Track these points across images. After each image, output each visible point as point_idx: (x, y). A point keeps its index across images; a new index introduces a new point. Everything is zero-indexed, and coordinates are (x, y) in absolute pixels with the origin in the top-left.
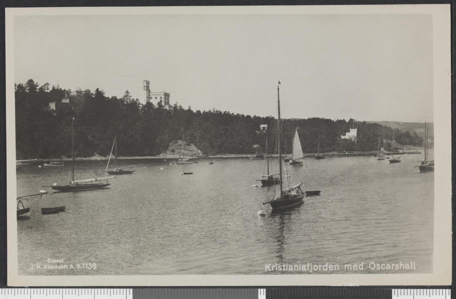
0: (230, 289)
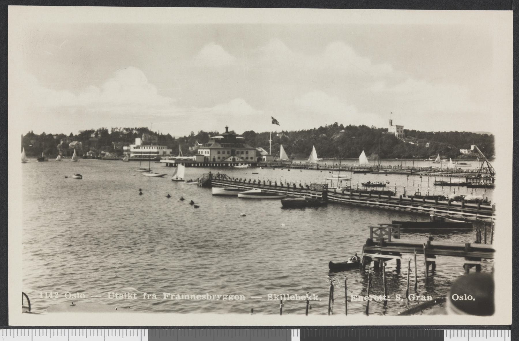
0: (259, 330)
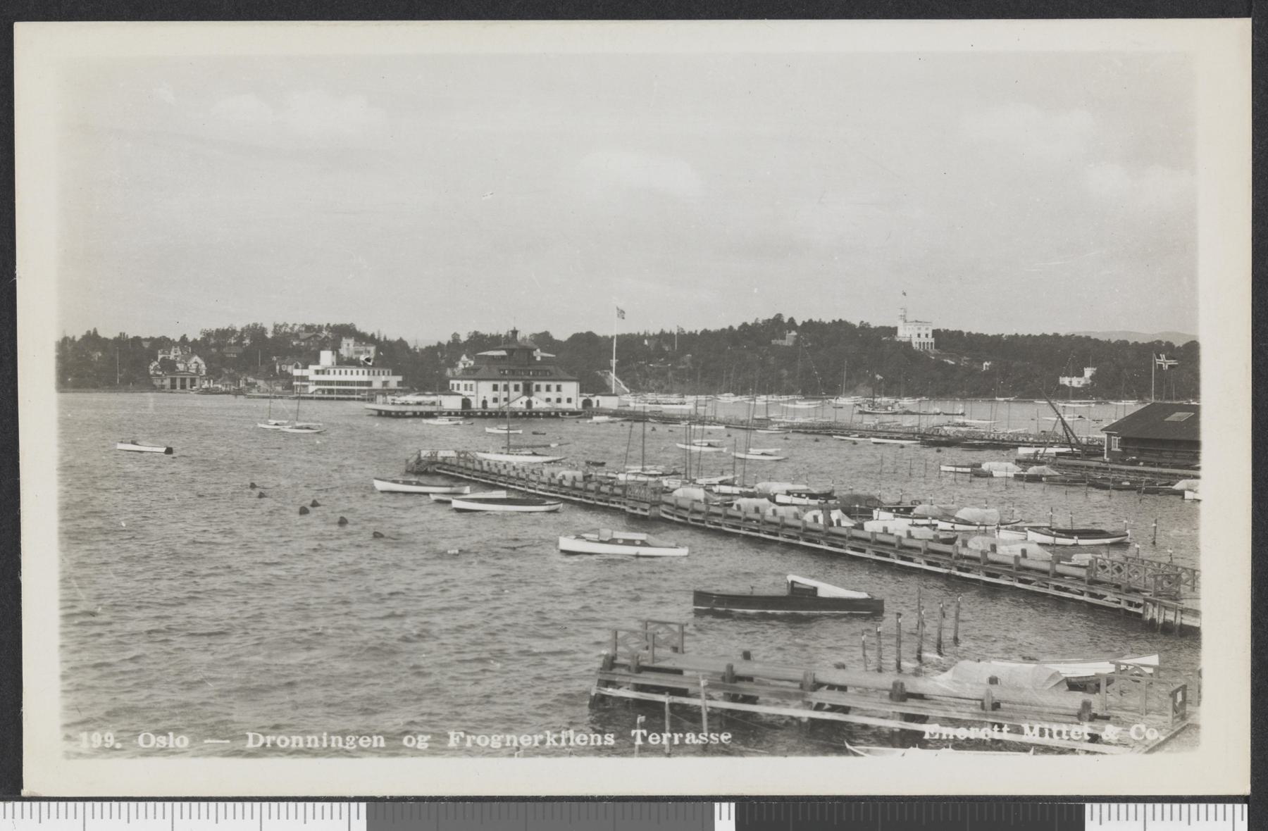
0: (637, 805)
